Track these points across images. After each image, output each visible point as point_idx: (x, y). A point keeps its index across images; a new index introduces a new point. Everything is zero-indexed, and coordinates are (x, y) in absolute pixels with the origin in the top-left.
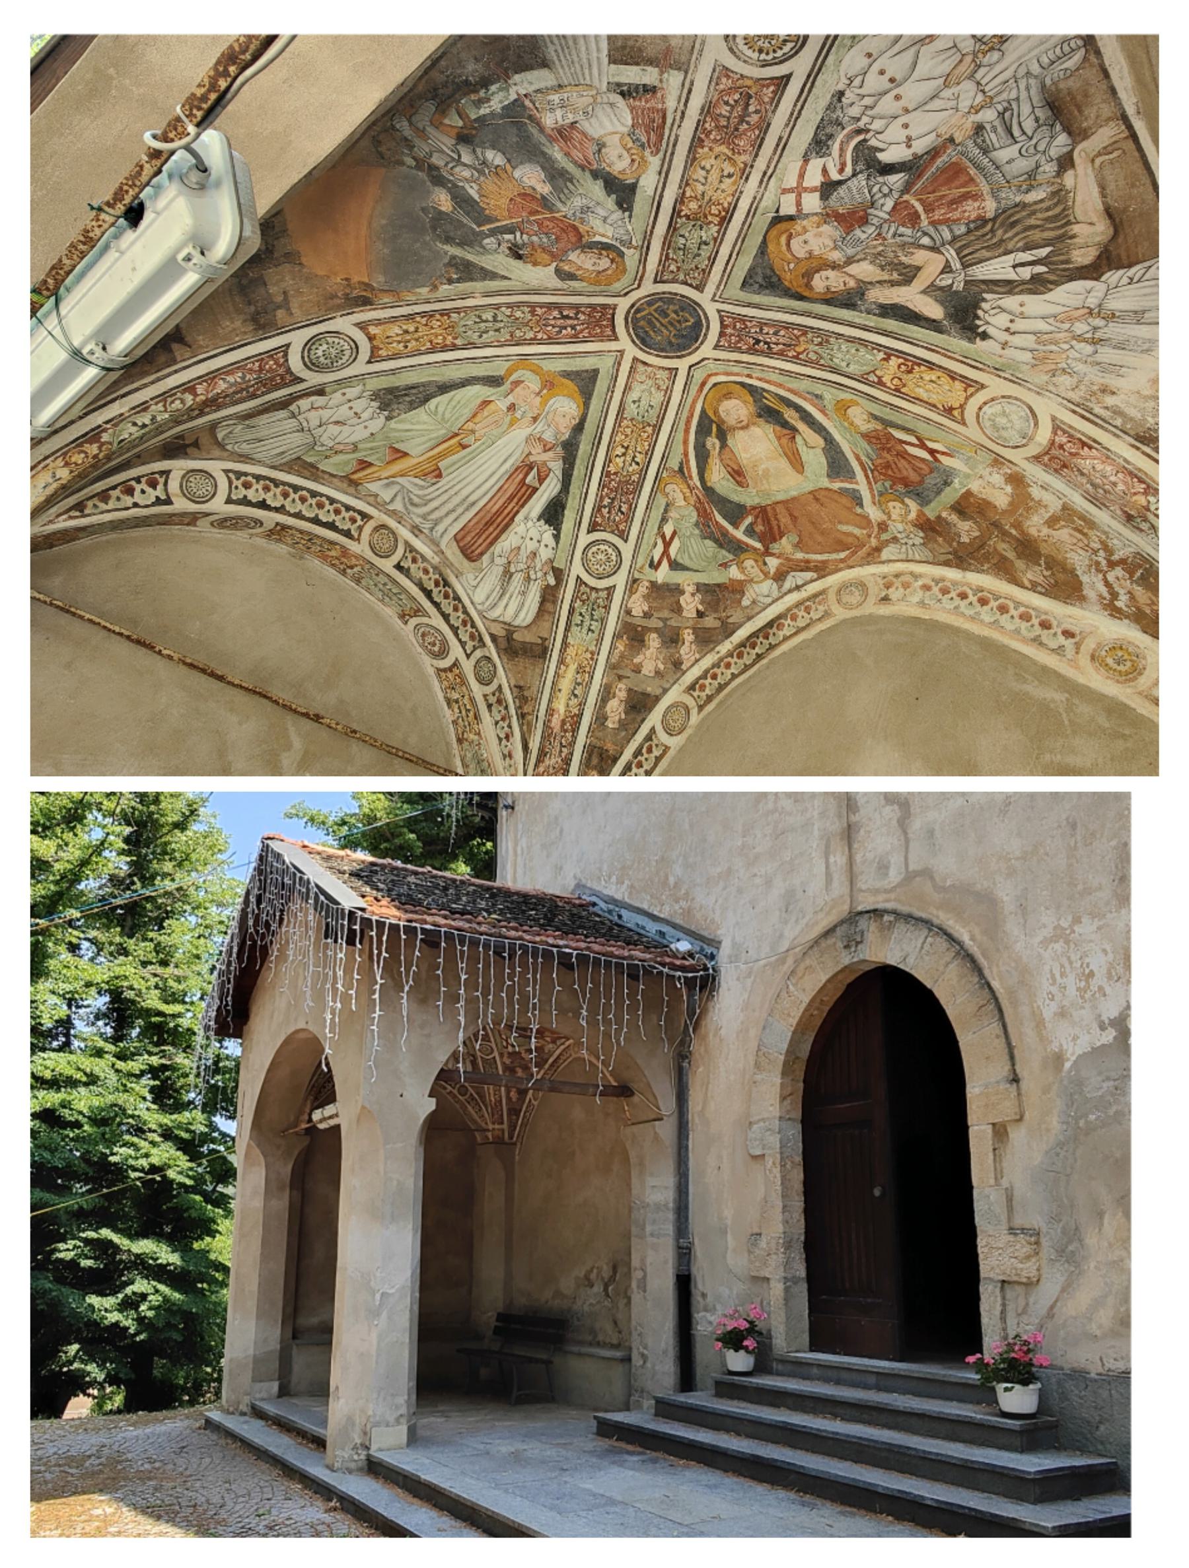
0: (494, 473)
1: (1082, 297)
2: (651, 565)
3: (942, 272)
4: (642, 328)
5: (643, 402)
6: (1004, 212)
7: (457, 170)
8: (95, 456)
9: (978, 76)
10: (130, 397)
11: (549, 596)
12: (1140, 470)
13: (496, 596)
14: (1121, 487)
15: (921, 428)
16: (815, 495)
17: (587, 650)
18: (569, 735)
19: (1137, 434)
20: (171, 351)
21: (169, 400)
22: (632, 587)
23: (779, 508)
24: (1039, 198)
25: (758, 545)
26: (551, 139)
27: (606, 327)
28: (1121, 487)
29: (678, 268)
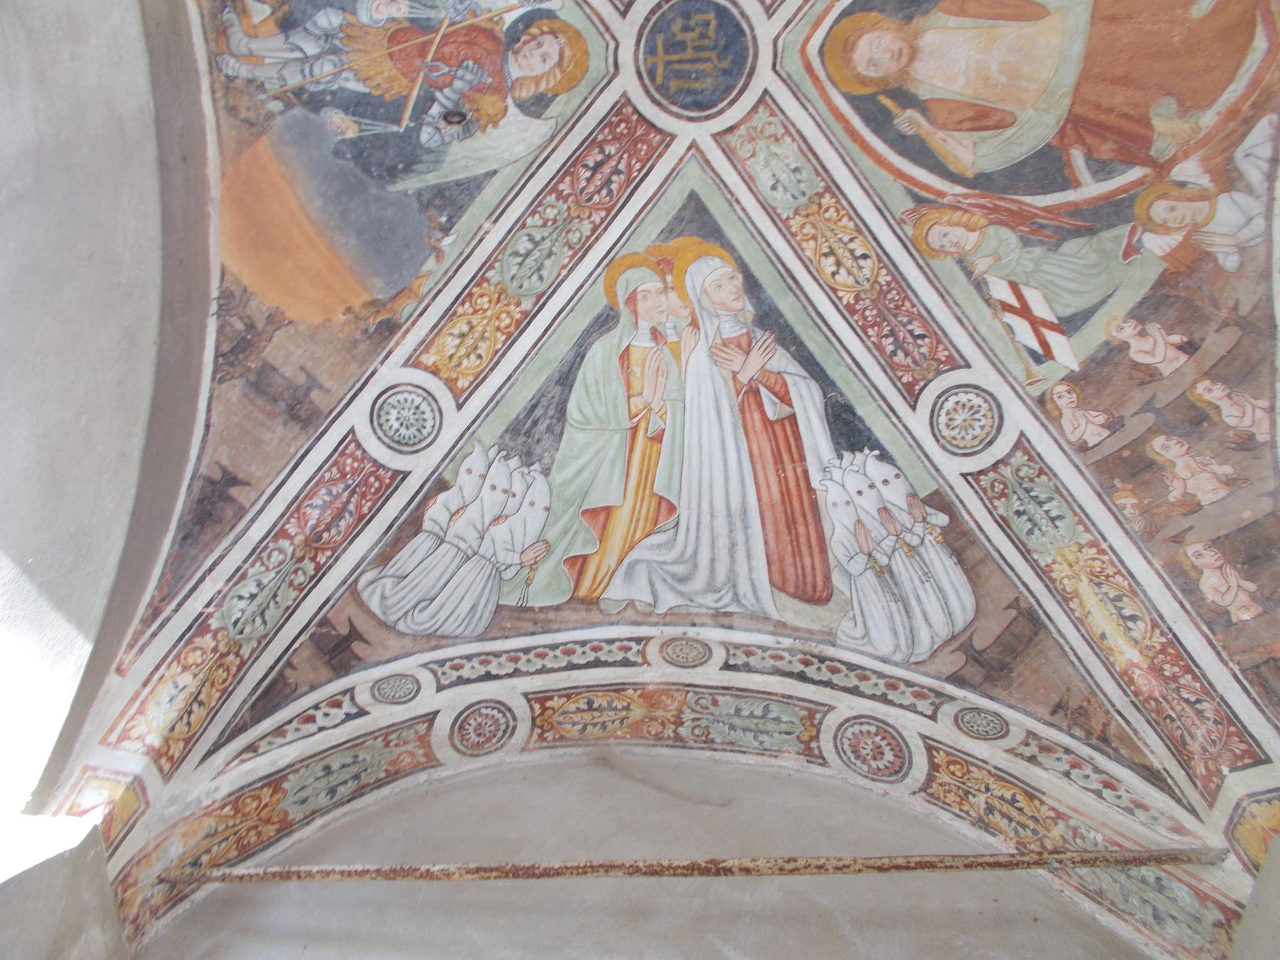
0: (723, 442)
2: (1038, 359)
4: (680, 91)
5: (783, 177)
7: (316, 70)
8: (215, 650)
10: (218, 568)
11: (959, 540)
13: (904, 615)
17: (1080, 547)
20: (231, 500)
21: (264, 555)
22: (1047, 414)
25: (1136, 173)
27: (647, 134)
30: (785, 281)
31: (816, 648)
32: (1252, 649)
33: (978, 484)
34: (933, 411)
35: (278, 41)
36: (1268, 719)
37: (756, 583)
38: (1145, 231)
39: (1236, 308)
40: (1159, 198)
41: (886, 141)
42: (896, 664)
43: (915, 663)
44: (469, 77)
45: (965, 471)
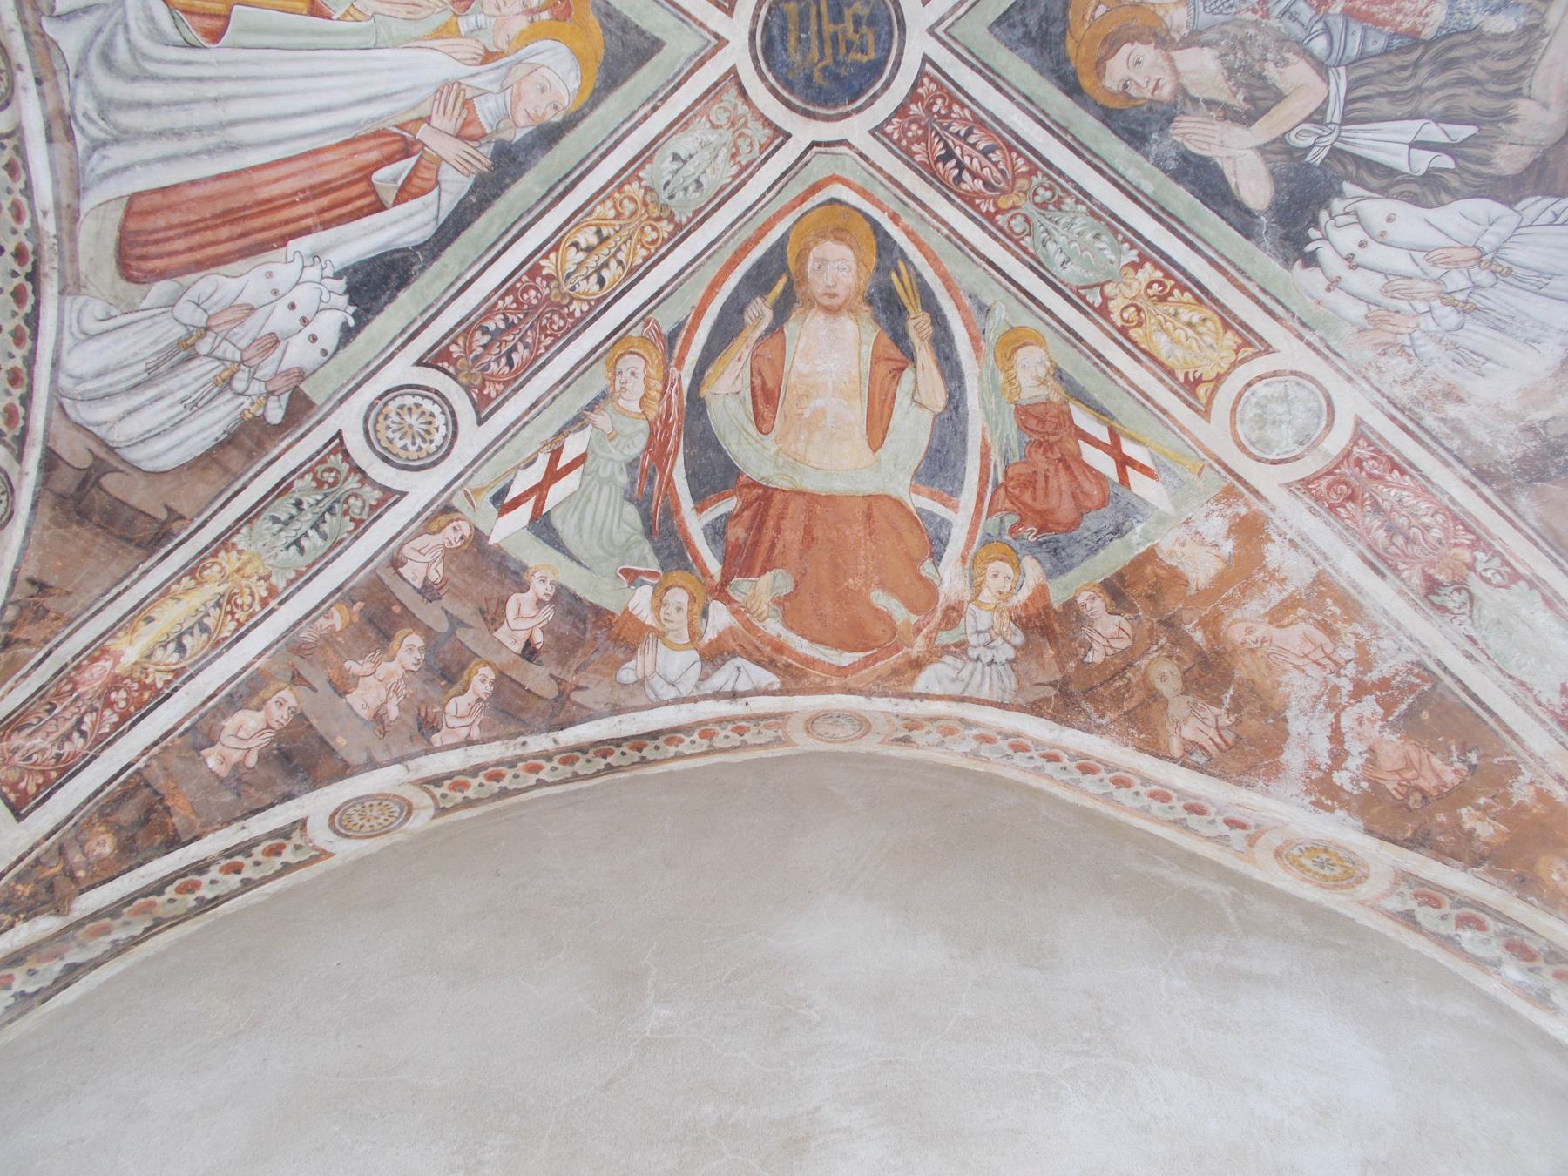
0: (328, 109)
2: (497, 498)
3: (1308, 120)
4: (784, 18)
5: (690, 168)
6: (1448, 36)
11: (248, 440)
12: (1470, 515)
14: (1437, 533)
15: (1127, 412)
16: (875, 507)
17: (266, 578)
18: (111, 717)
19: (1477, 466)
23: (796, 506)
25: (715, 567)
28: (1437, 533)
30: (560, 181)
31: (50, 267)
32: (169, 776)
33: (330, 453)
34: (418, 387)
36: (79, 808)
37: (128, 174)
38: (654, 586)
39: (578, 688)
40: (690, 594)
41: (736, 290)
42: (54, 381)
43: (62, 407)
45: (345, 435)
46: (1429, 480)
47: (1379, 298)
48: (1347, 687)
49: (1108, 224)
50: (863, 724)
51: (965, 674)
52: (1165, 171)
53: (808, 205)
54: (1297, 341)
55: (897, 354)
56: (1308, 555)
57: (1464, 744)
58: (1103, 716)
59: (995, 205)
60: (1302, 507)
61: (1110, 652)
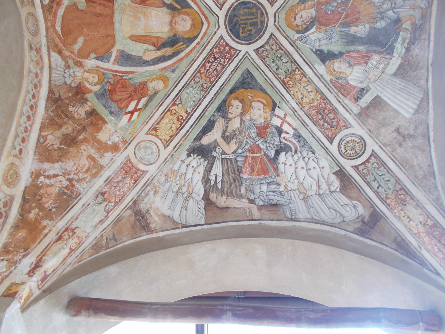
1: (197, 193)
3: (223, 150)
4: (252, 8)
6: (241, 179)
7: (390, 5)
9: (297, 192)
12: (124, 200)
14: (118, 193)
15: (147, 112)
23: (108, 11)
24: (241, 191)
26: (368, 52)
29: (272, 49)
35: (402, 15)
44: (330, 8)
46: (132, 190)
47: (180, 172)
48: (71, 177)
49: (197, 104)
50: (36, 33)
51: (59, 68)
52: (211, 117)
53: (201, 16)
54: (168, 154)
55: (159, 45)
56: (109, 163)
57: (57, 207)
58: (51, 112)
59: (203, 73)
60: (123, 160)
61: (73, 113)
